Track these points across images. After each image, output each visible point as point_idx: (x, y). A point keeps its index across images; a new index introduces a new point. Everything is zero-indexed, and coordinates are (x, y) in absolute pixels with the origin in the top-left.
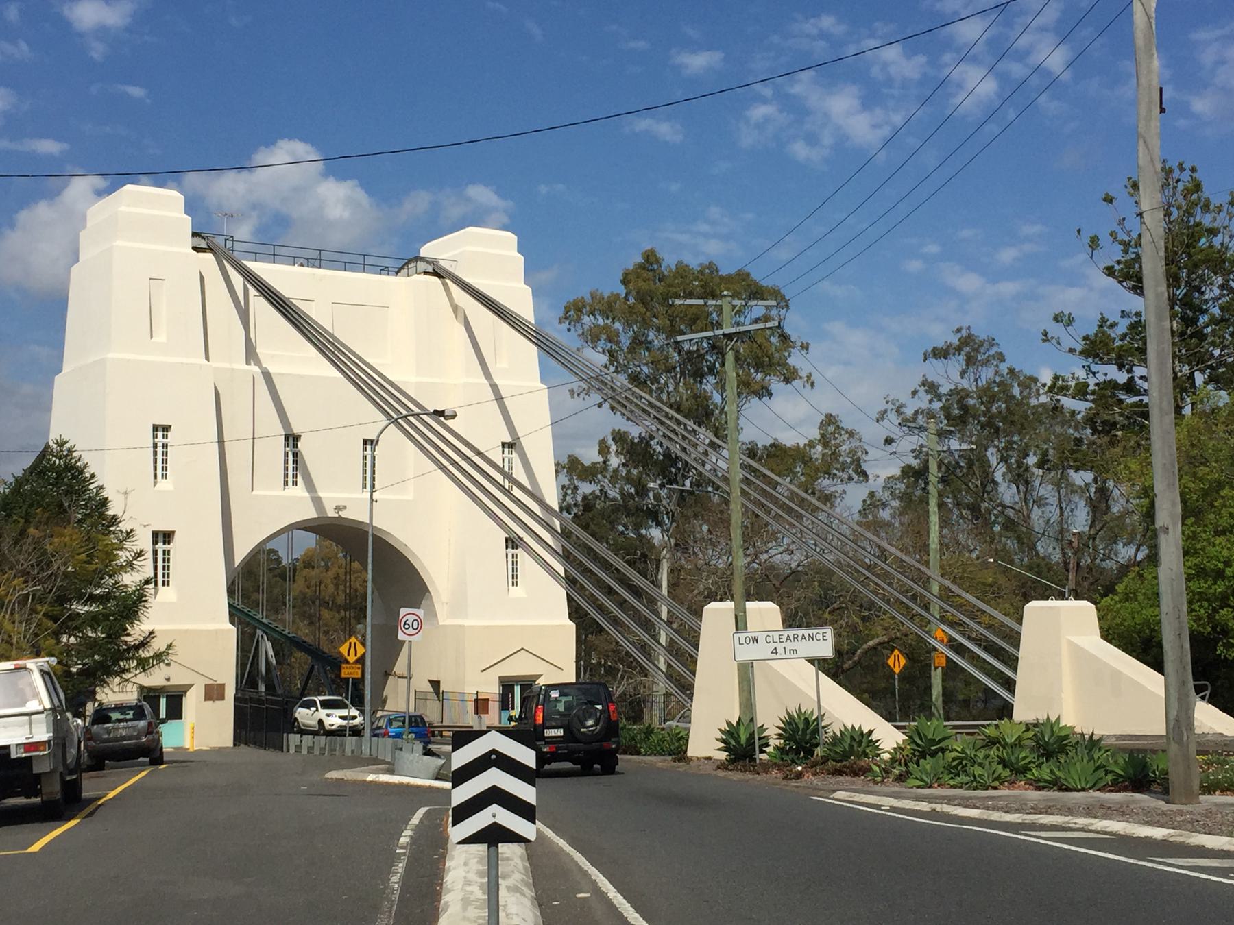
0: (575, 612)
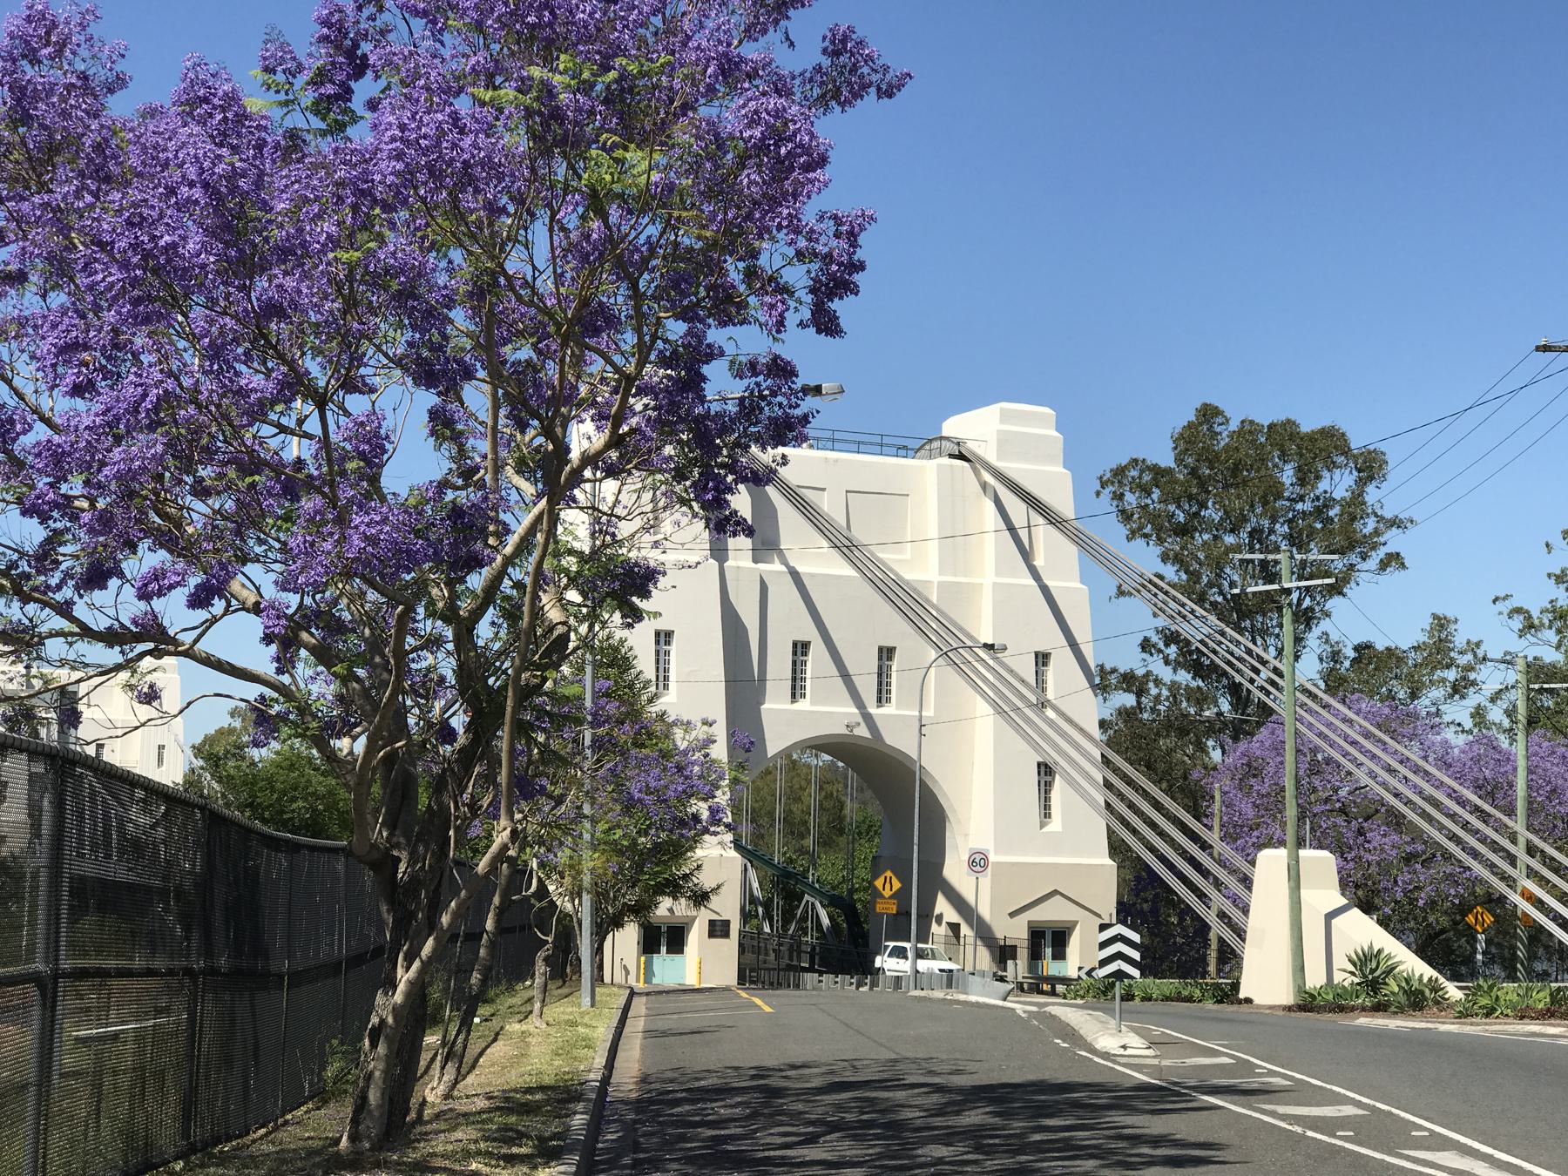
0: (1116, 848)
